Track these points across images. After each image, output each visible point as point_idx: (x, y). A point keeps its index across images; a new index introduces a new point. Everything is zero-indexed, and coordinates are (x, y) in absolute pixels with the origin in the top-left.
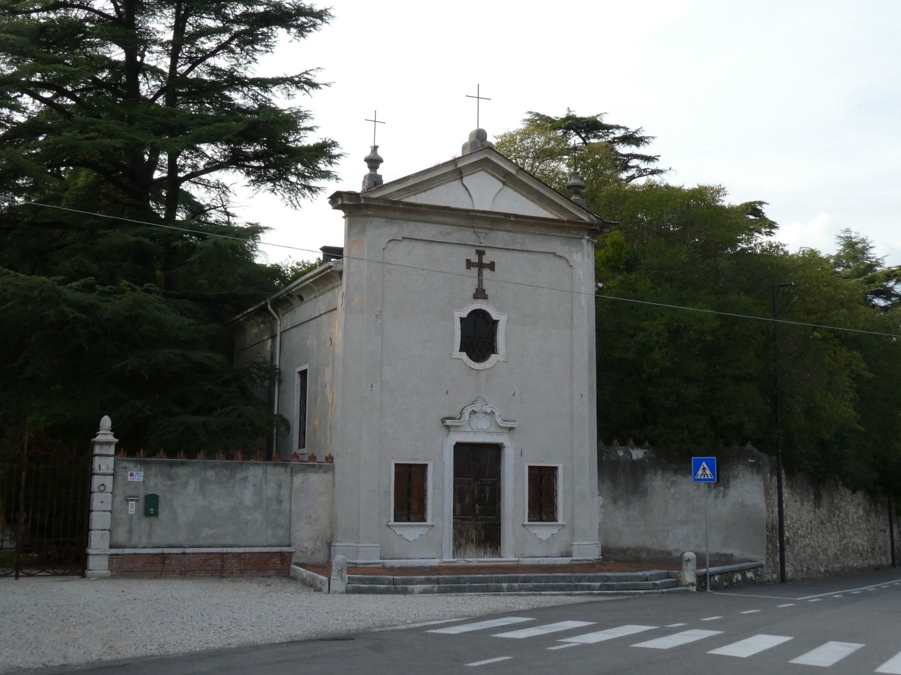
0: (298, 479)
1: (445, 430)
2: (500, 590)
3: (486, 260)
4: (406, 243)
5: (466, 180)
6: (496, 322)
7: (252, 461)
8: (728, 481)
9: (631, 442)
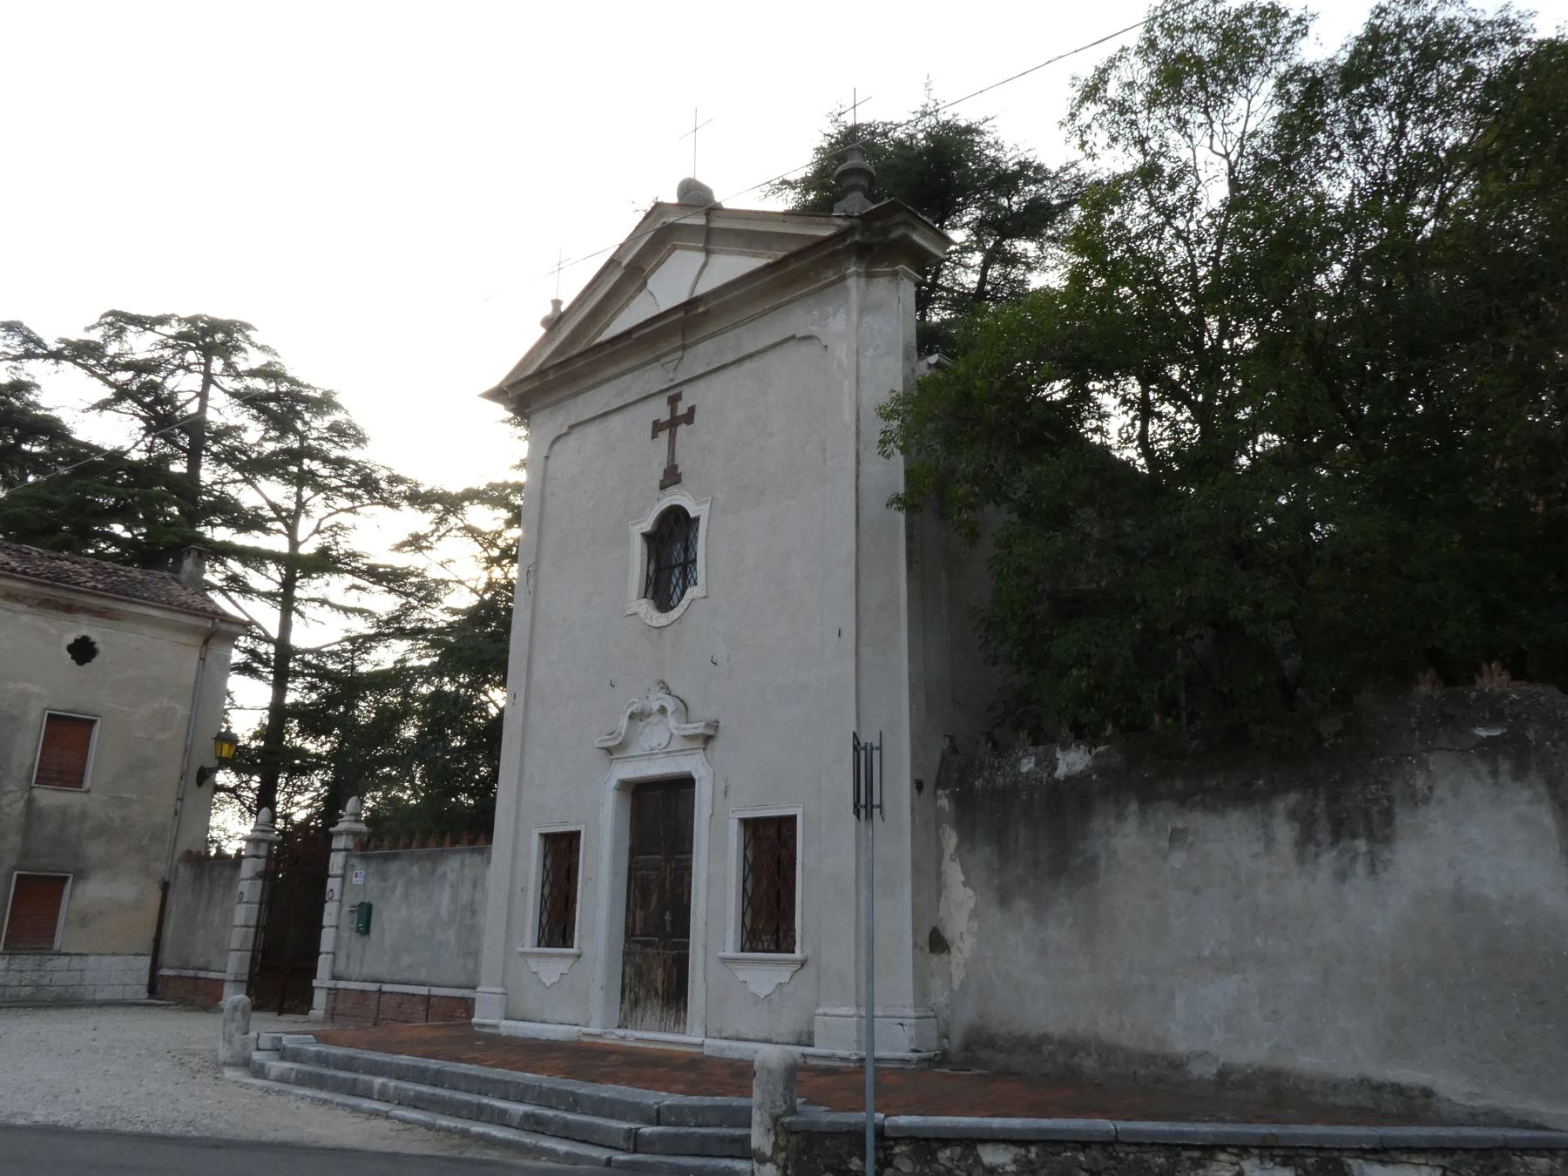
4: (576, 434)
8: (1388, 816)
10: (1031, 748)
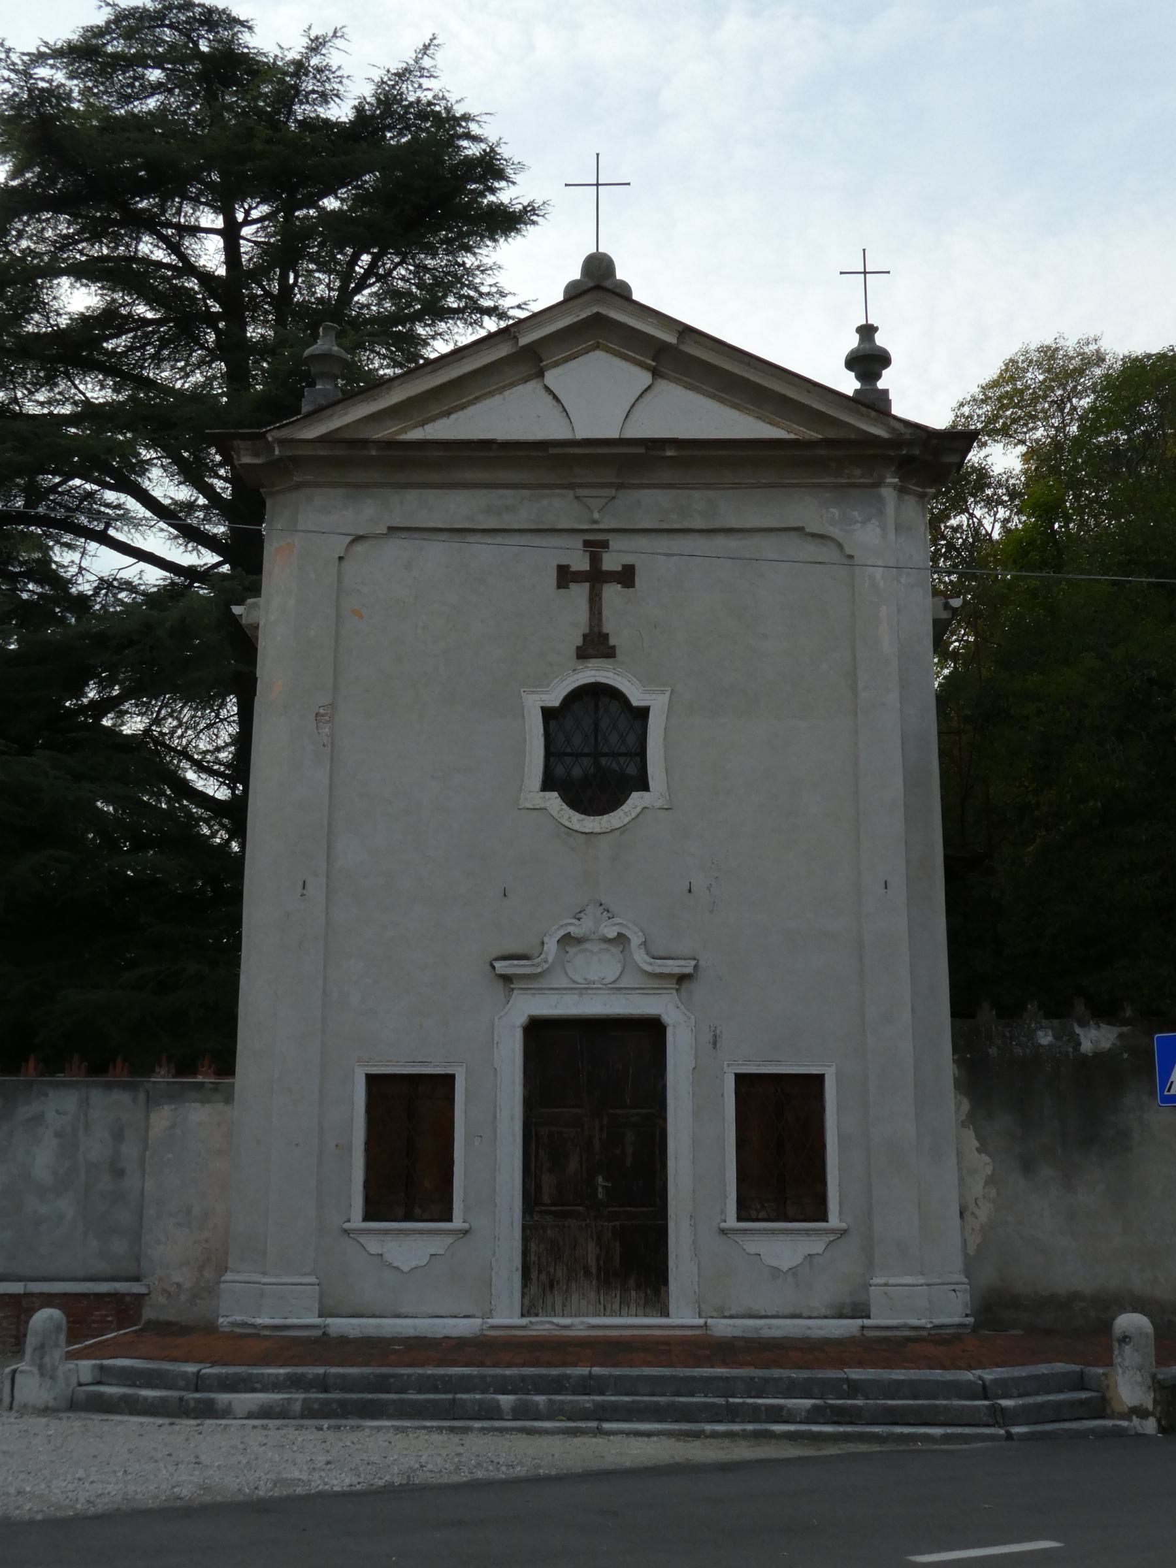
0: (162, 1118)
1: (499, 985)
2: (491, 1412)
3: (611, 562)
5: (551, 377)
6: (643, 714)
7: (60, 1077)
9: (1080, 1007)
10: (1044, 1022)
